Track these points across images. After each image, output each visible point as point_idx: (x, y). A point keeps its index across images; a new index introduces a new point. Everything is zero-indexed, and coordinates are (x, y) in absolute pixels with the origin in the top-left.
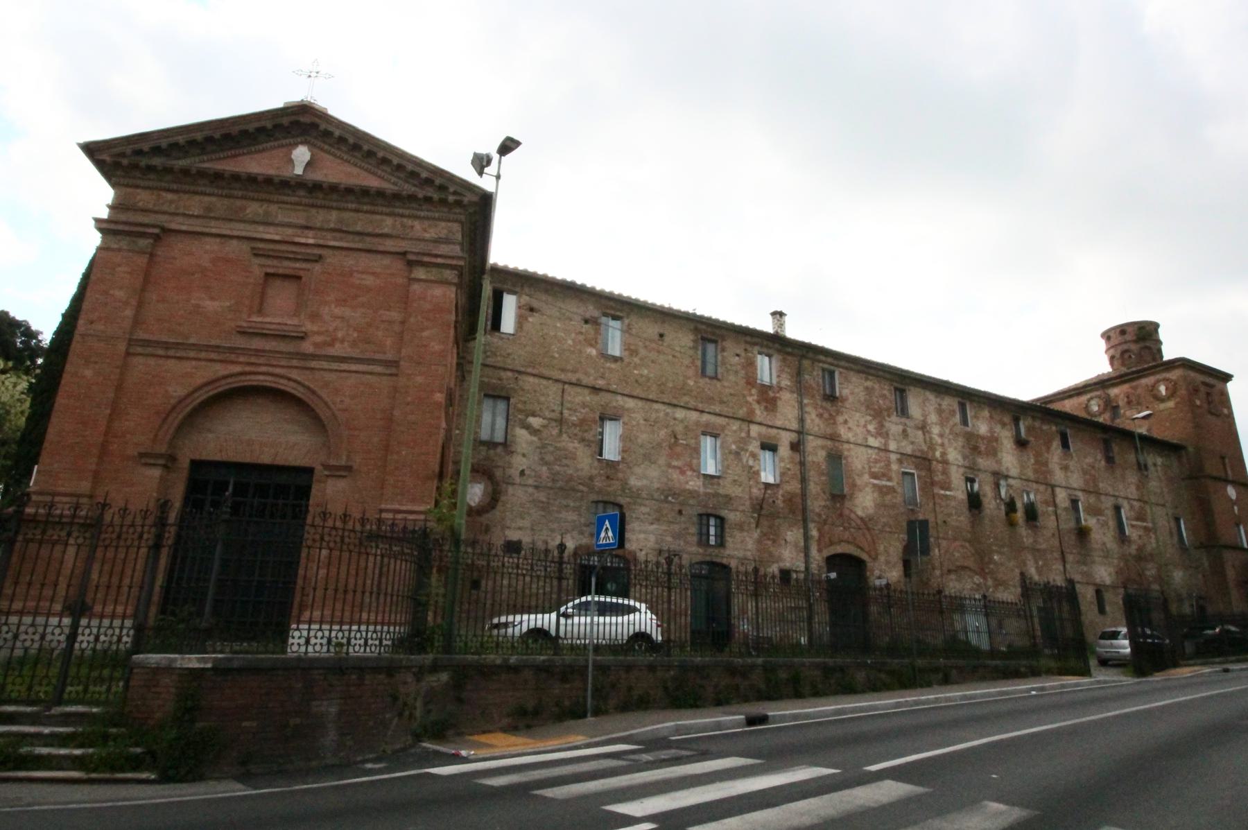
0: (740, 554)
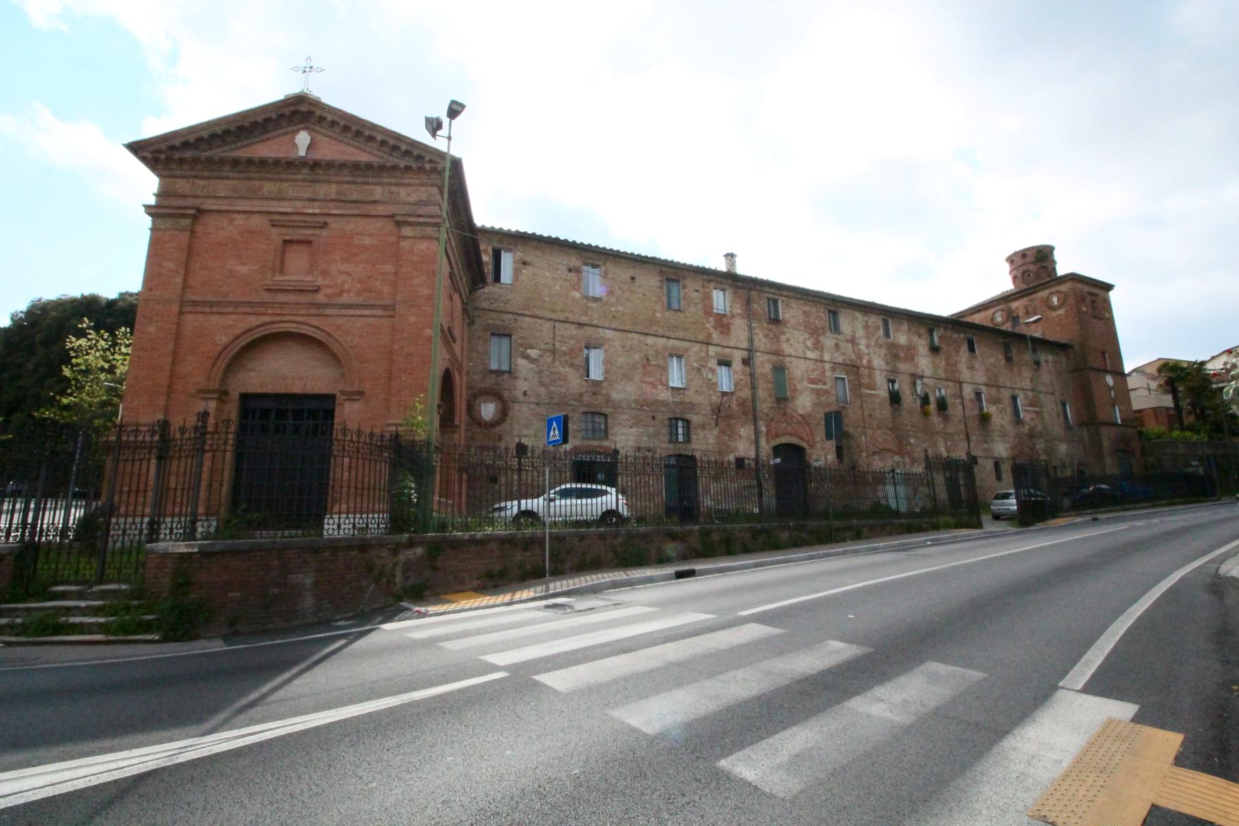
0: (704, 447)
